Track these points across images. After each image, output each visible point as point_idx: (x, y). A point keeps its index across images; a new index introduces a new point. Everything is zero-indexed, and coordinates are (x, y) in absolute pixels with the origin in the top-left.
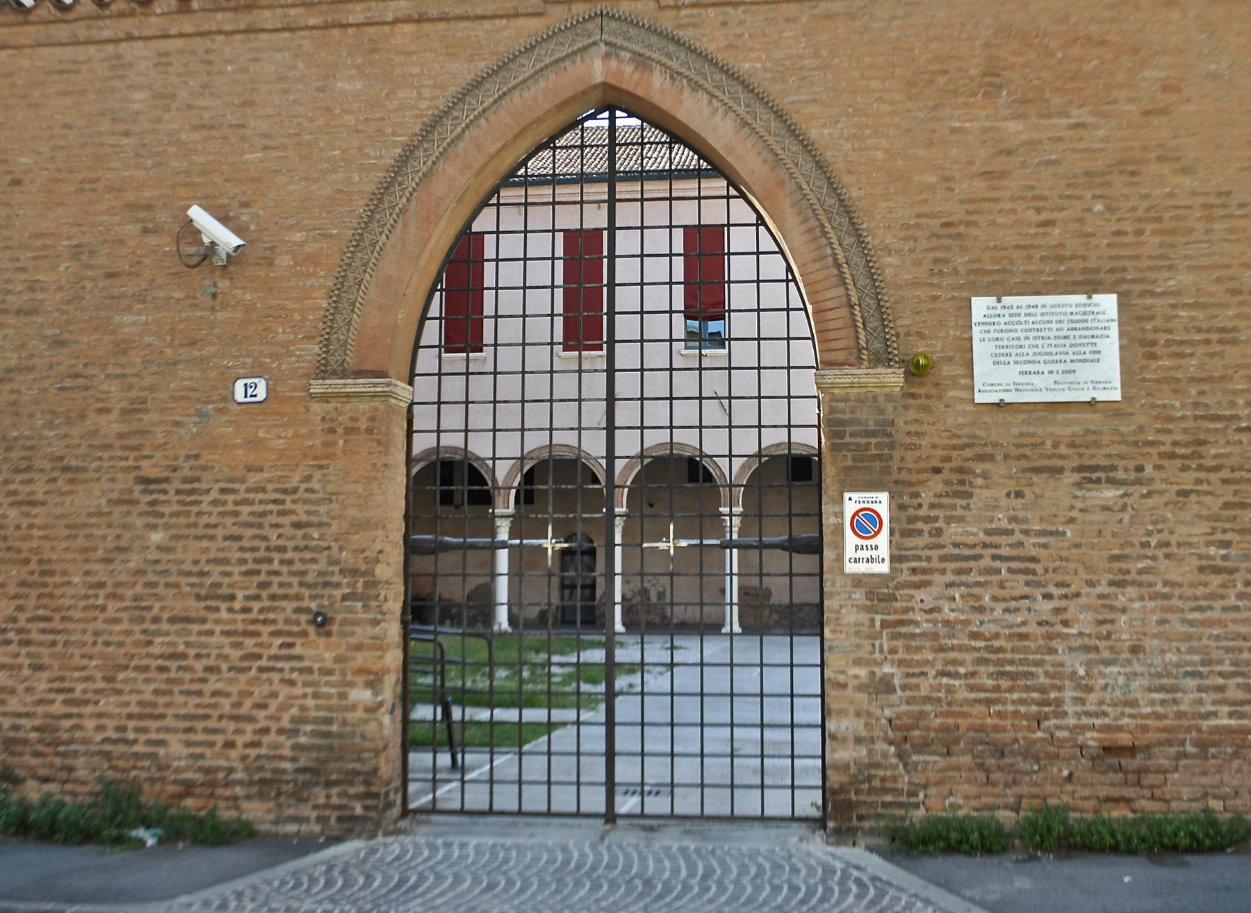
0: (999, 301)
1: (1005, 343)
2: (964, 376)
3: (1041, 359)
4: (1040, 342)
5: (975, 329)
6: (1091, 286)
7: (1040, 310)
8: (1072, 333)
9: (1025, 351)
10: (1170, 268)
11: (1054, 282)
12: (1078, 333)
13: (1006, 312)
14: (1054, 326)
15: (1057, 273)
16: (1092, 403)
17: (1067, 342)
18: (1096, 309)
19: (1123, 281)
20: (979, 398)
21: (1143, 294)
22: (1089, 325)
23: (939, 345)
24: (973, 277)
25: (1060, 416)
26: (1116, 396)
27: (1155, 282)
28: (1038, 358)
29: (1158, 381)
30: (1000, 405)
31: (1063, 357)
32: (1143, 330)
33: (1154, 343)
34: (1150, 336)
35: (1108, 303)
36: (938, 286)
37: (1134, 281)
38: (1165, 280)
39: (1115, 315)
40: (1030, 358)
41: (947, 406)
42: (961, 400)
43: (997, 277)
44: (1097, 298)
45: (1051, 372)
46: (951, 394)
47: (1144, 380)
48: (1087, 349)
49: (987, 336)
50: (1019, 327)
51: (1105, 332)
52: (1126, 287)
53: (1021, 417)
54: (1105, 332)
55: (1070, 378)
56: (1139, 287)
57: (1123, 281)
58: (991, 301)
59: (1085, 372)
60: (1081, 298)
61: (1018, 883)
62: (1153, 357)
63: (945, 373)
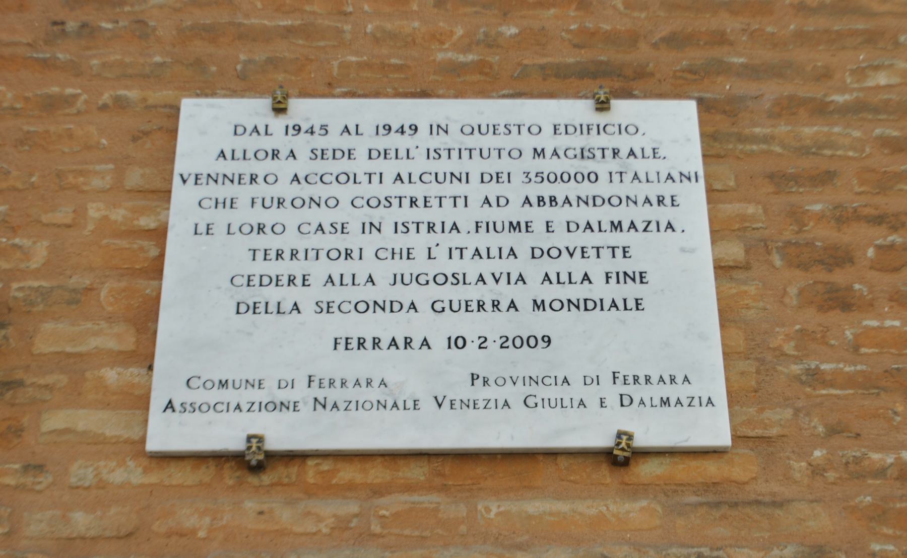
0: (279, 109)
1: (288, 242)
2: (124, 358)
3: (423, 295)
4: (419, 241)
5: (183, 196)
6: (608, 79)
7: (424, 139)
8: (538, 215)
9: (362, 269)
10: (871, 38)
11: (481, 67)
12: (559, 215)
13: (302, 144)
15: (491, 43)
16: (620, 458)
17: (522, 242)
18: (624, 143)
19: (721, 69)
20: (164, 433)
21: (787, 108)
22: (603, 189)
23: (40, 252)
24: (199, 48)
25: (492, 509)
26: (713, 428)
27: (825, 75)
28: (405, 294)
29: (867, 384)
30: (253, 463)
31: (505, 293)
32: (797, 215)
33: (839, 257)
34: (823, 234)
35: (670, 127)
36: (75, 70)
37: (752, 72)
38: (860, 73)
39: (695, 163)
40: (382, 292)
41: (35, 468)
42: (96, 445)
43: (283, 49)
44: (624, 110)
45: (458, 343)
46: (54, 421)
47: (815, 377)
48: (597, 268)
49: (221, 217)
51: (663, 214)
52: (727, 86)
53: (331, 509)
54: (663, 214)
55: (530, 362)
56: (772, 90)
57: (721, 69)
58: (253, 109)
59: (586, 345)
60: (579, 110)
61: (165, 92)
62: (840, 301)
63: (42, 346)
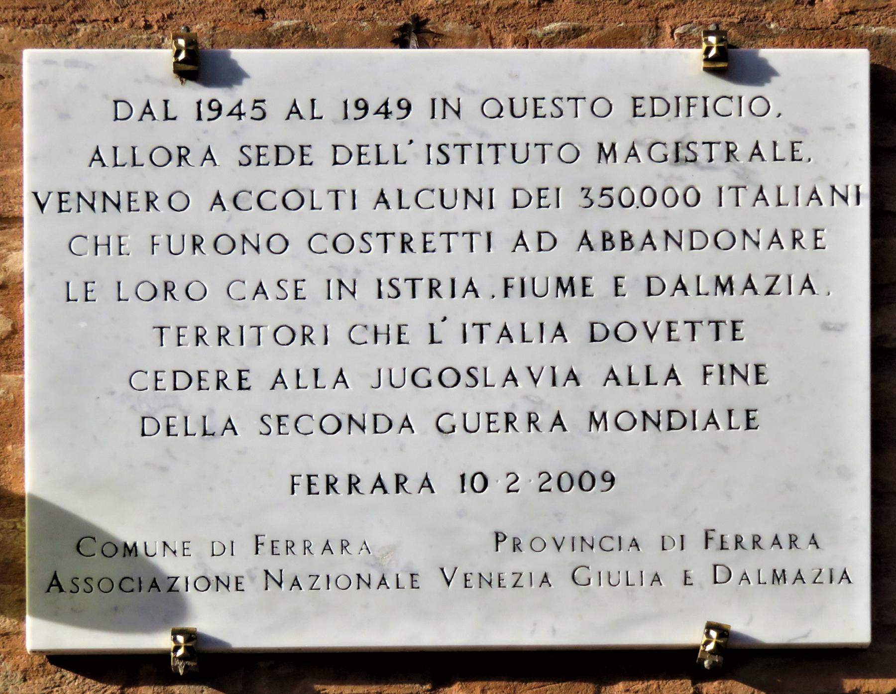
1: (214, 312)
4: (416, 311)
8: (601, 266)
9: (329, 359)
12: (635, 265)
14: (503, 221)
22: (706, 217)
31: (550, 399)
40: (353, 400)
48: (689, 356)
49: (105, 269)
50: (296, 225)
51: (793, 262)
54: (793, 262)
55: (582, 513)
